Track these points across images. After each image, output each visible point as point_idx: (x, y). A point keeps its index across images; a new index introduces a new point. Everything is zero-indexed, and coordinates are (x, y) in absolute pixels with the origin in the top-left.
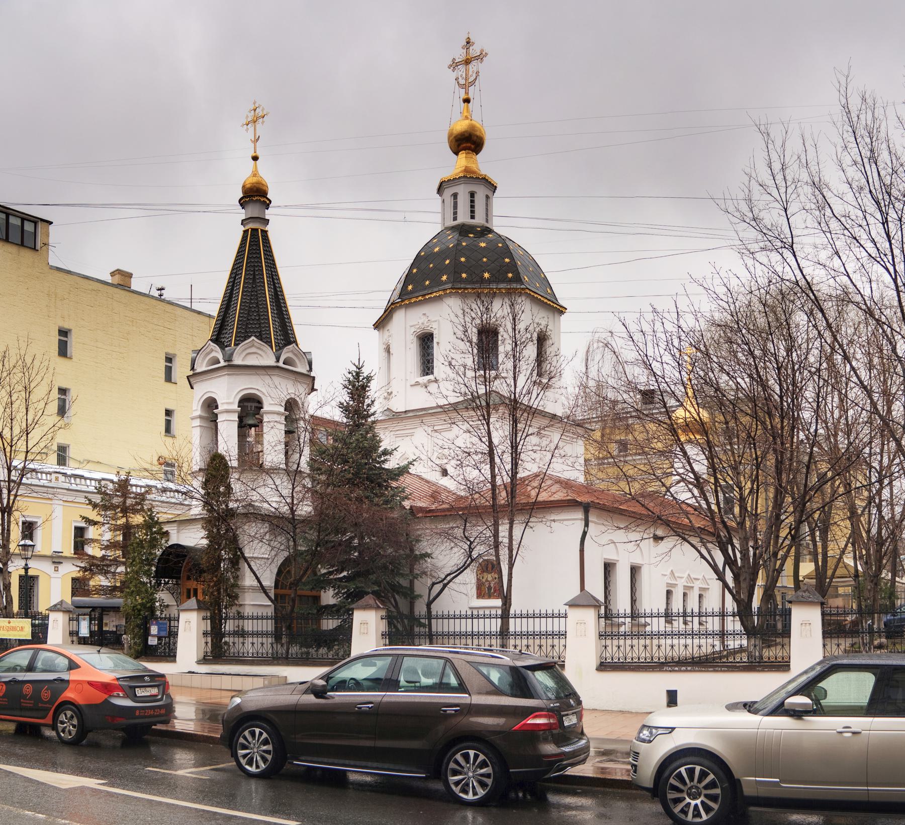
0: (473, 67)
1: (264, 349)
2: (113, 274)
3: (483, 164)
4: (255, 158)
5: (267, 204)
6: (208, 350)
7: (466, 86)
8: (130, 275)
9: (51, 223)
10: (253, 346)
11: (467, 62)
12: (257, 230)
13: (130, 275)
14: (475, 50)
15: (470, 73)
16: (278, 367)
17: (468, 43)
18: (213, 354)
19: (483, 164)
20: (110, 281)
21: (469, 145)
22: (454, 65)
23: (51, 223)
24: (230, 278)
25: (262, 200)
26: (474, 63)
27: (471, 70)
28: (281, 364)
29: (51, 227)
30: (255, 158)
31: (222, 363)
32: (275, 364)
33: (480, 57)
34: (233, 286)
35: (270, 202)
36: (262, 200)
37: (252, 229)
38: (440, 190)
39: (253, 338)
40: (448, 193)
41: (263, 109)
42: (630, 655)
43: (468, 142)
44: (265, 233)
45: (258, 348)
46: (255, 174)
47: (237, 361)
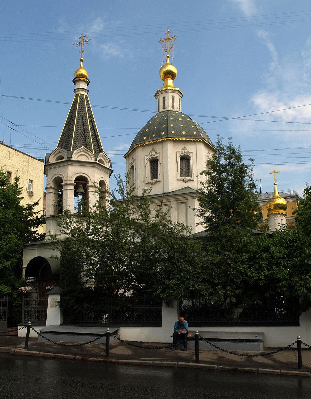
28: (97, 162)
33: (173, 38)
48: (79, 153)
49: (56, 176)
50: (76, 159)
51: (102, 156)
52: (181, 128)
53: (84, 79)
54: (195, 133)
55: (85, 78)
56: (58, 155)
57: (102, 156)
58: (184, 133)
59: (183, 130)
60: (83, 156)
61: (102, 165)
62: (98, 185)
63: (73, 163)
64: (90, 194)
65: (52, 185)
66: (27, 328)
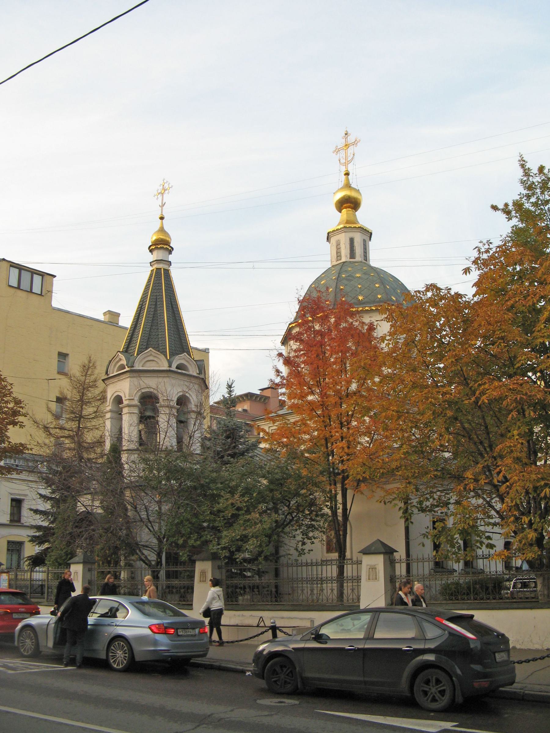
0: (351, 150)
1: (159, 357)
2: (105, 314)
3: (363, 217)
4: (162, 218)
5: (170, 251)
6: (117, 359)
7: (346, 164)
8: (118, 315)
9: (55, 276)
10: (151, 355)
11: (347, 146)
12: (161, 269)
13: (118, 315)
14: (351, 139)
15: (349, 154)
16: (170, 371)
17: (346, 134)
18: (121, 362)
19: (363, 217)
20: (103, 320)
21: (349, 204)
22: (337, 151)
23: (55, 276)
24: (139, 305)
25: (165, 247)
26: (351, 147)
27: (349, 152)
28: (174, 368)
29: (54, 279)
30: (162, 218)
31: (127, 369)
32: (168, 369)
33: (355, 143)
34: (140, 310)
35: (173, 249)
36: (165, 247)
37: (157, 269)
38: (328, 239)
39: (185, 353)
40: (333, 240)
41: (169, 184)
42: (351, 597)
43: (350, 203)
44: (167, 272)
45: (155, 357)
46: (162, 230)
47: (137, 367)
48: (145, 358)
49: (147, 390)
50: (141, 368)
51: (184, 359)
52: (358, 290)
53: (162, 246)
54: (379, 296)
55: (163, 244)
56: (117, 366)
57: (184, 359)
58: (360, 298)
59: (360, 294)
60: (151, 362)
61: (184, 372)
62: (174, 403)
63: (115, 380)
64: (162, 420)
65: (136, 402)
66: (270, 631)
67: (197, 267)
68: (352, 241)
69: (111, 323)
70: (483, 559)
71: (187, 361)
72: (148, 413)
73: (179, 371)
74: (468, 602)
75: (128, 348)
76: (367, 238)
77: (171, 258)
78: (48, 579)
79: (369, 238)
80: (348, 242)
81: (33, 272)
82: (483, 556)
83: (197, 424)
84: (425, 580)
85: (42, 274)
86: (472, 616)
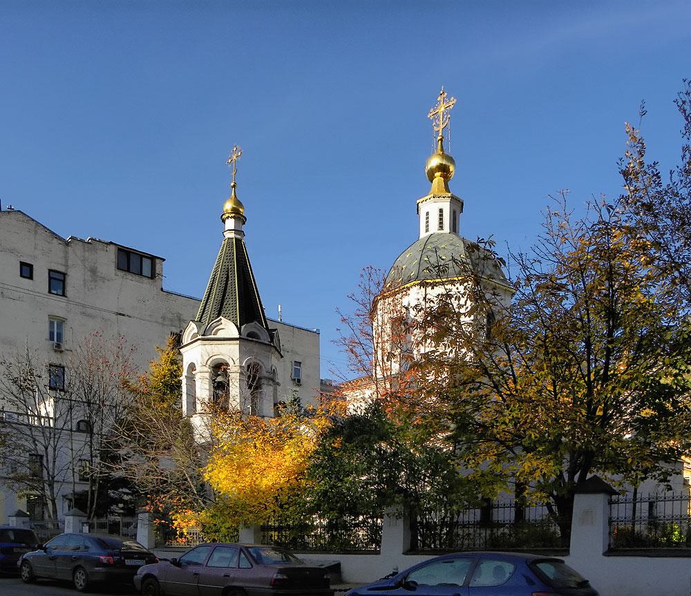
23: (164, 260)
51: (255, 327)
56: (191, 335)
67: (441, 219)
68: (441, 211)
69: (89, 311)
70: (681, 500)
71: (258, 329)
72: (219, 379)
73: (250, 339)
74: (642, 548)
75: (201, 317)
76: (458, 211)
77: (244, 228)
78: (634, 518)
79: (459, 209)
80: (438, 213)
81: (142, 256)
82: (665, 498)
83: (374, 375)
84: (683, 521)
85: (153, 259)
86: (336, 568)
